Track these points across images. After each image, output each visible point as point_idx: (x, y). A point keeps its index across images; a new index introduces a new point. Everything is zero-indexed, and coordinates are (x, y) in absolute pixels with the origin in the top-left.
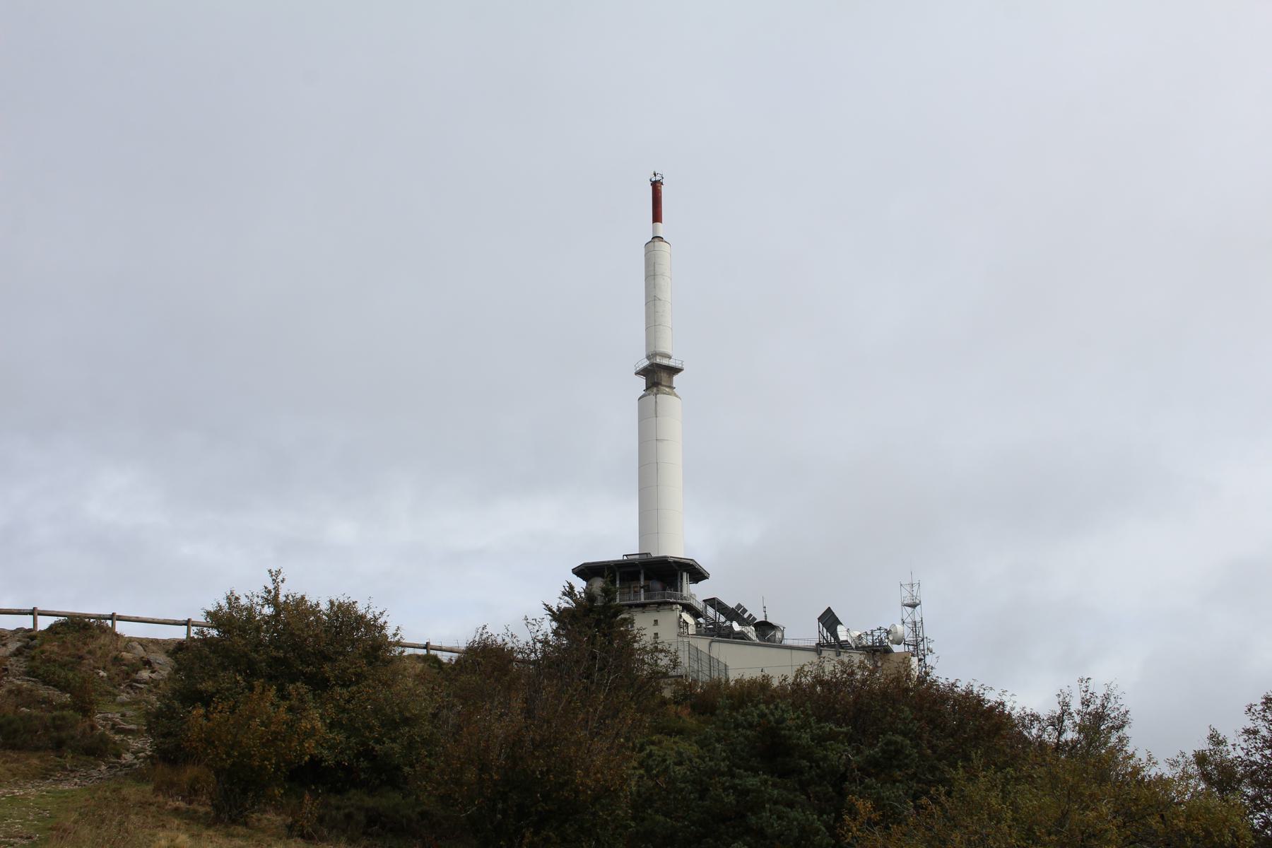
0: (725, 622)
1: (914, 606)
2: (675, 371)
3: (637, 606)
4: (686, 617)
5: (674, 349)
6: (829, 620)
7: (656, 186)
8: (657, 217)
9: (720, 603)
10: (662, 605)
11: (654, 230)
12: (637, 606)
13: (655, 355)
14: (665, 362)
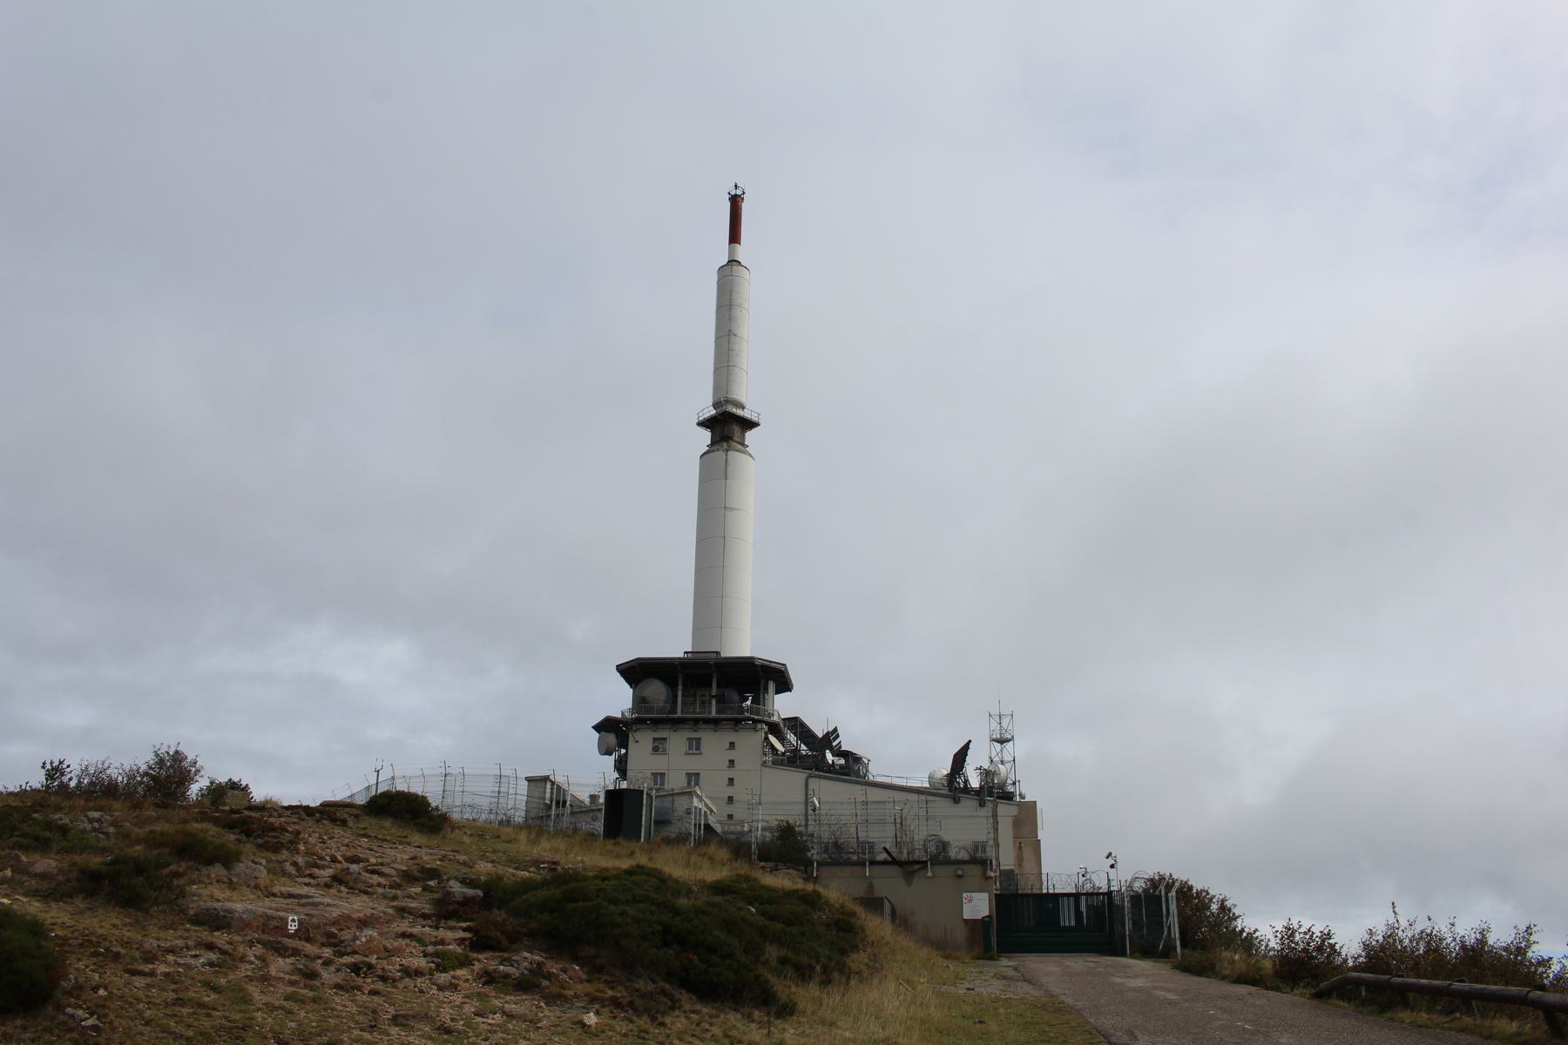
0: (817, 754)
1: (1002, 741)
2: (750, 424)
3: (707, 721)
5: (751, 398)
7: (735, 202)
8: (735, 237)
9: (803, 725)
11: (731, 252)
12: (707, 721)
13: (728, 401)
14: (739, 412)
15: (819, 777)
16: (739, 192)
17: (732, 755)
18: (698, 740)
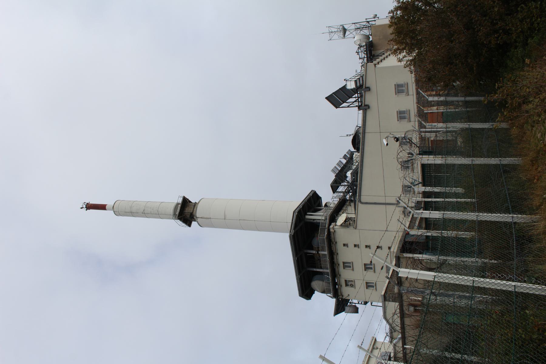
0: (348, 177)
1: (345, 30)
4: (341, 219)
6: (338, 98)
7: (89, 207)
8: (102, 207)
10: (331, 240)
15: (360, 196)
16: (85, 206)
17: (351, 245)
18: (344, 263)
